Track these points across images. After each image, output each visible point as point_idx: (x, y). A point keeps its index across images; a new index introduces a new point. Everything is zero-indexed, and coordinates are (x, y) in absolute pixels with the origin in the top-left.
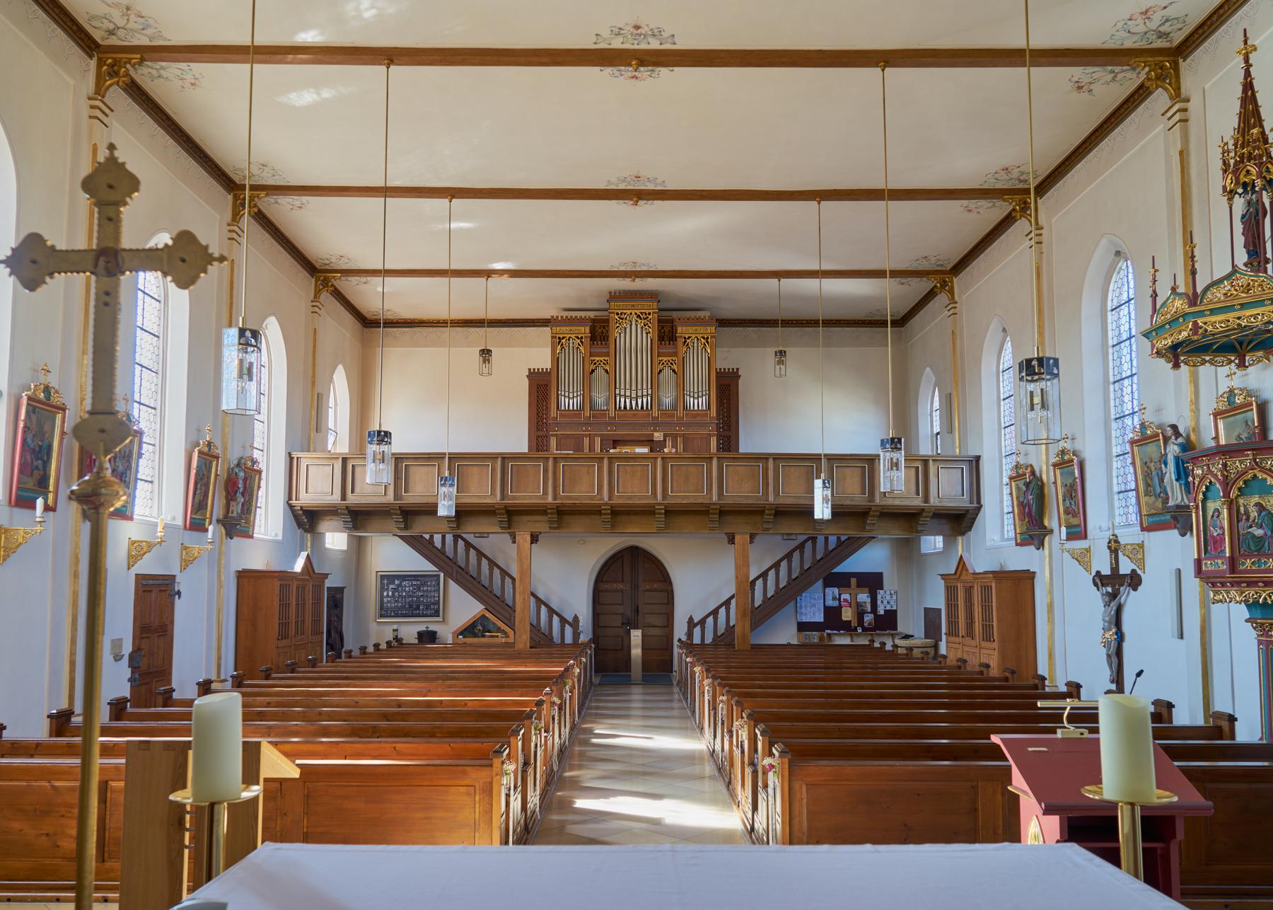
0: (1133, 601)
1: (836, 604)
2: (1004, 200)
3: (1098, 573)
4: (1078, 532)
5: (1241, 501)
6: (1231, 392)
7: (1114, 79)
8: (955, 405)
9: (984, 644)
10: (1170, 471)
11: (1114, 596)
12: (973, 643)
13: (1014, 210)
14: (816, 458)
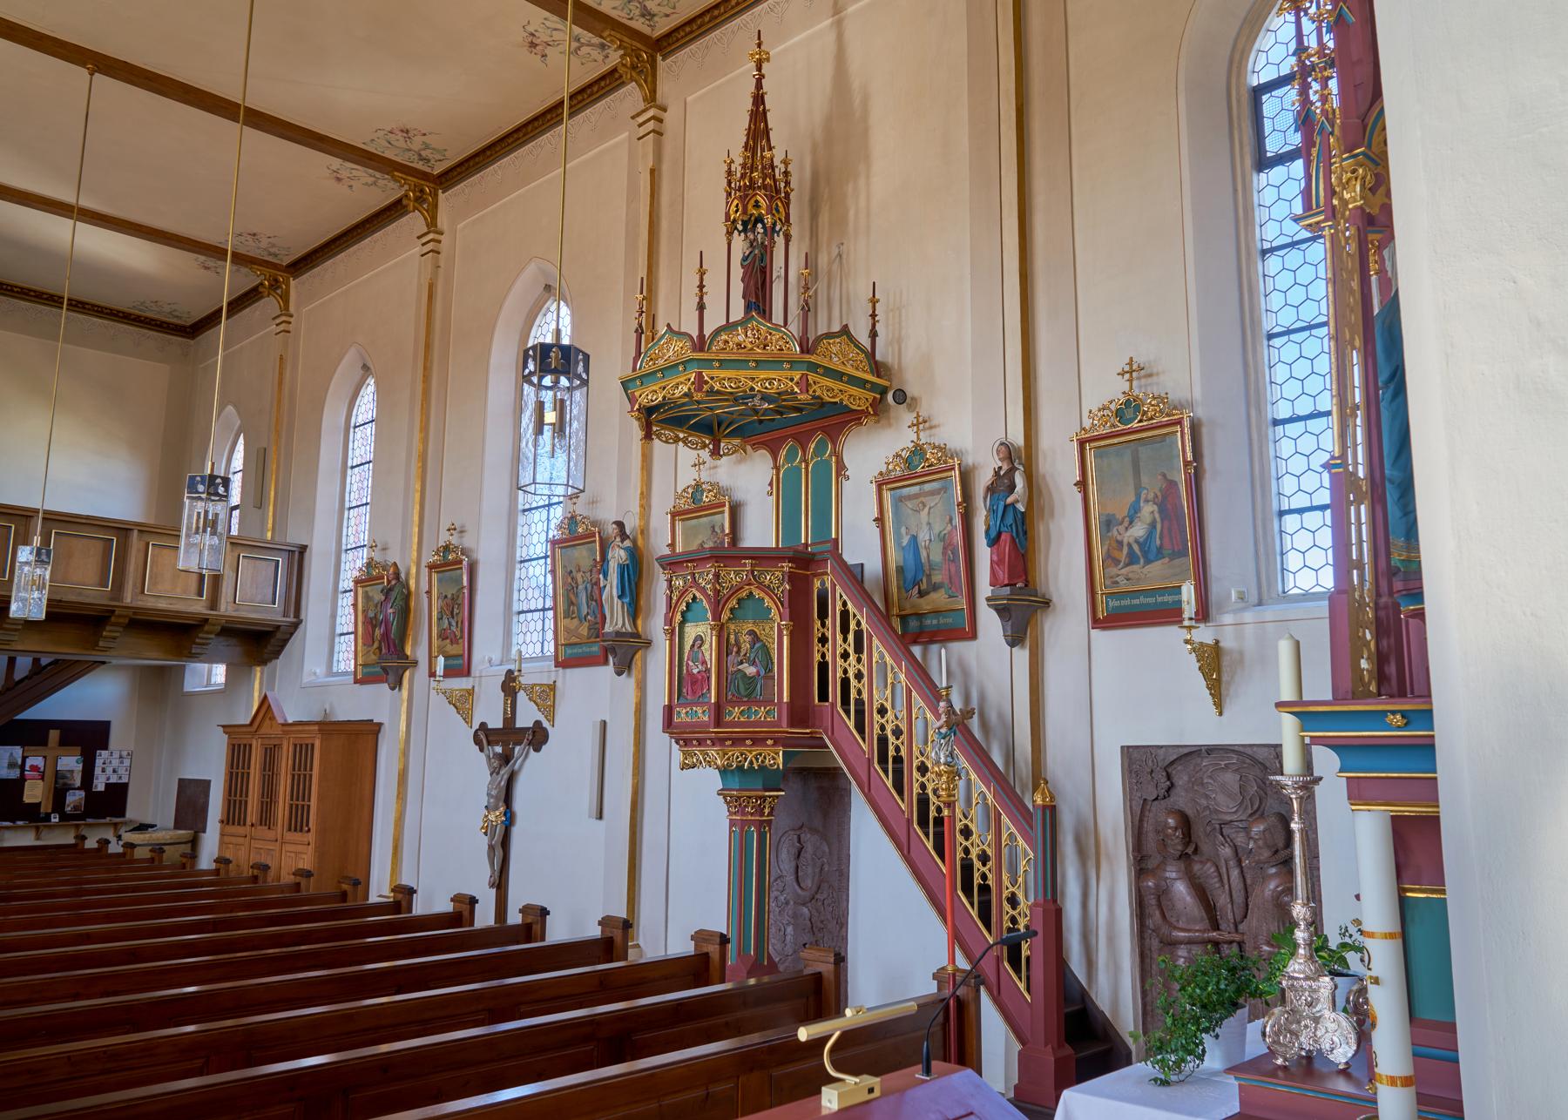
0: (533, 768)
1: (14, 774)
2: (394, 179)
3: (483, 725)
4: (460, 667)
5: (732, 627)
6: (698, 487)
7: (375, 183)
8: (272, 466)
9: (290, 836)
10: (611, 585)
11: (506, 758)
12: (270, 834)
13: (261, 284)
14: (23, 516)
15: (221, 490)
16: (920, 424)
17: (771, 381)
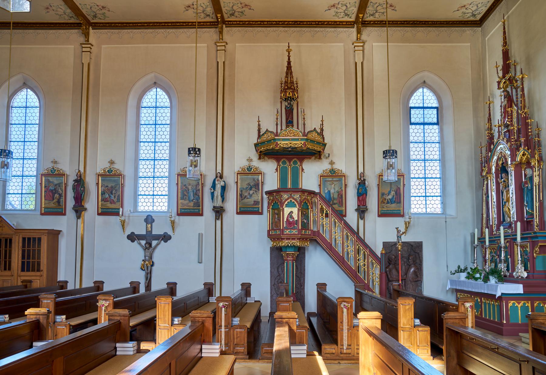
15: (198, 153)
16: (332, 163)
17: (296, 144)
